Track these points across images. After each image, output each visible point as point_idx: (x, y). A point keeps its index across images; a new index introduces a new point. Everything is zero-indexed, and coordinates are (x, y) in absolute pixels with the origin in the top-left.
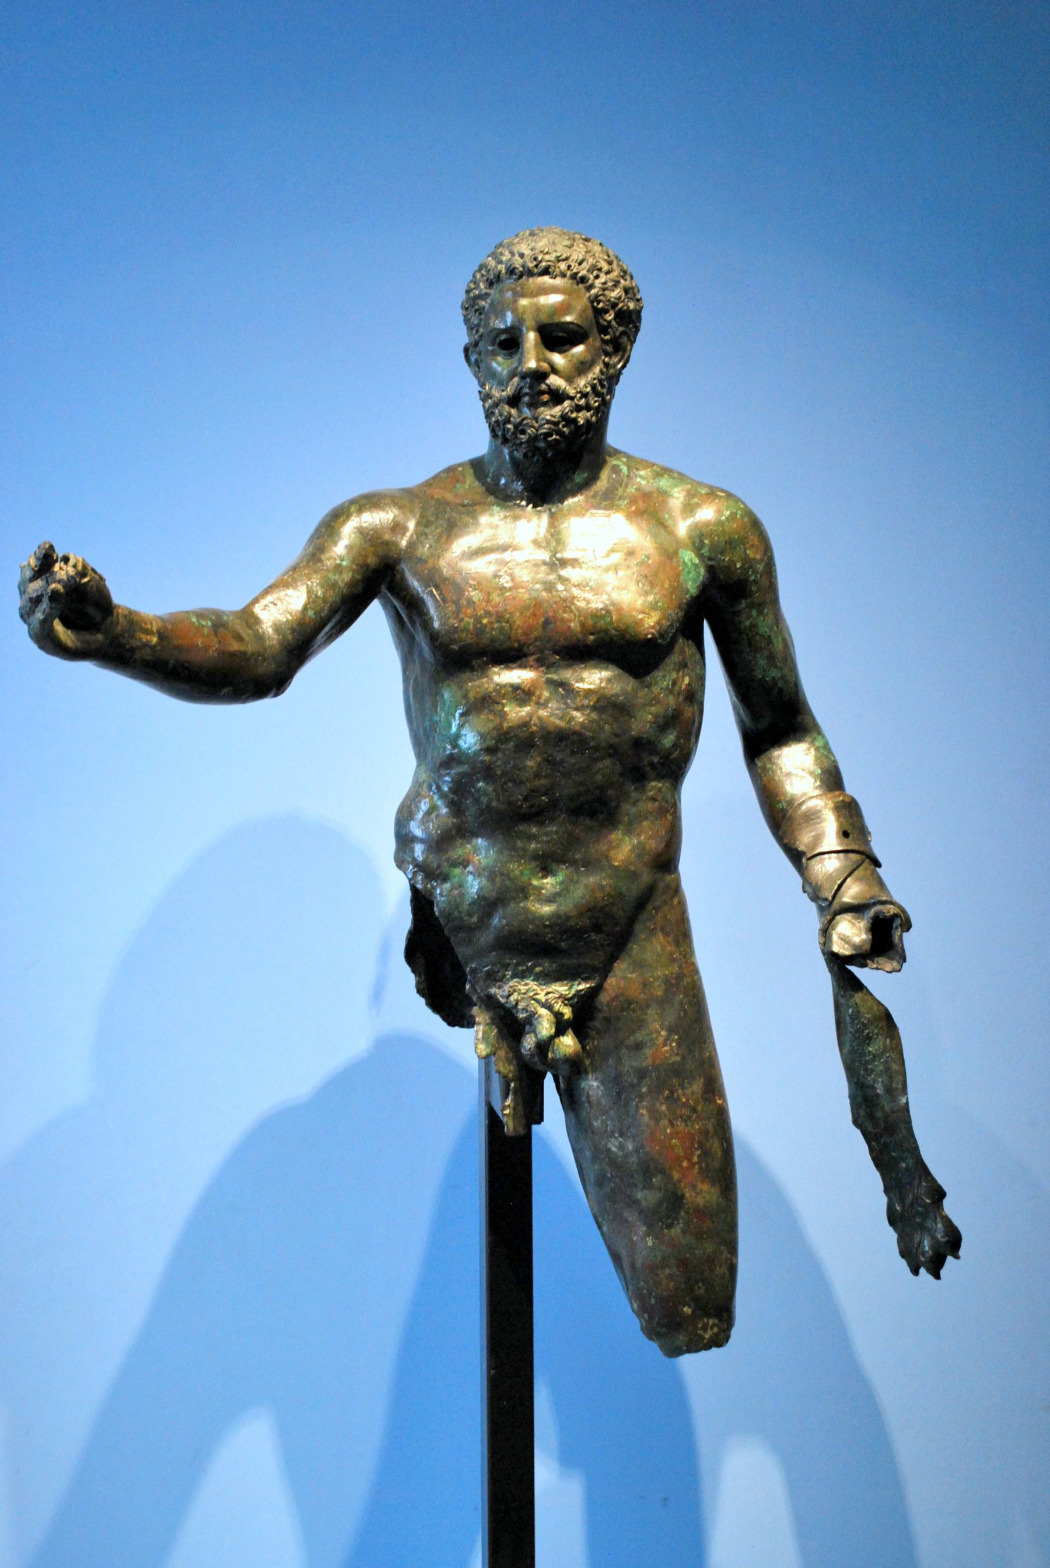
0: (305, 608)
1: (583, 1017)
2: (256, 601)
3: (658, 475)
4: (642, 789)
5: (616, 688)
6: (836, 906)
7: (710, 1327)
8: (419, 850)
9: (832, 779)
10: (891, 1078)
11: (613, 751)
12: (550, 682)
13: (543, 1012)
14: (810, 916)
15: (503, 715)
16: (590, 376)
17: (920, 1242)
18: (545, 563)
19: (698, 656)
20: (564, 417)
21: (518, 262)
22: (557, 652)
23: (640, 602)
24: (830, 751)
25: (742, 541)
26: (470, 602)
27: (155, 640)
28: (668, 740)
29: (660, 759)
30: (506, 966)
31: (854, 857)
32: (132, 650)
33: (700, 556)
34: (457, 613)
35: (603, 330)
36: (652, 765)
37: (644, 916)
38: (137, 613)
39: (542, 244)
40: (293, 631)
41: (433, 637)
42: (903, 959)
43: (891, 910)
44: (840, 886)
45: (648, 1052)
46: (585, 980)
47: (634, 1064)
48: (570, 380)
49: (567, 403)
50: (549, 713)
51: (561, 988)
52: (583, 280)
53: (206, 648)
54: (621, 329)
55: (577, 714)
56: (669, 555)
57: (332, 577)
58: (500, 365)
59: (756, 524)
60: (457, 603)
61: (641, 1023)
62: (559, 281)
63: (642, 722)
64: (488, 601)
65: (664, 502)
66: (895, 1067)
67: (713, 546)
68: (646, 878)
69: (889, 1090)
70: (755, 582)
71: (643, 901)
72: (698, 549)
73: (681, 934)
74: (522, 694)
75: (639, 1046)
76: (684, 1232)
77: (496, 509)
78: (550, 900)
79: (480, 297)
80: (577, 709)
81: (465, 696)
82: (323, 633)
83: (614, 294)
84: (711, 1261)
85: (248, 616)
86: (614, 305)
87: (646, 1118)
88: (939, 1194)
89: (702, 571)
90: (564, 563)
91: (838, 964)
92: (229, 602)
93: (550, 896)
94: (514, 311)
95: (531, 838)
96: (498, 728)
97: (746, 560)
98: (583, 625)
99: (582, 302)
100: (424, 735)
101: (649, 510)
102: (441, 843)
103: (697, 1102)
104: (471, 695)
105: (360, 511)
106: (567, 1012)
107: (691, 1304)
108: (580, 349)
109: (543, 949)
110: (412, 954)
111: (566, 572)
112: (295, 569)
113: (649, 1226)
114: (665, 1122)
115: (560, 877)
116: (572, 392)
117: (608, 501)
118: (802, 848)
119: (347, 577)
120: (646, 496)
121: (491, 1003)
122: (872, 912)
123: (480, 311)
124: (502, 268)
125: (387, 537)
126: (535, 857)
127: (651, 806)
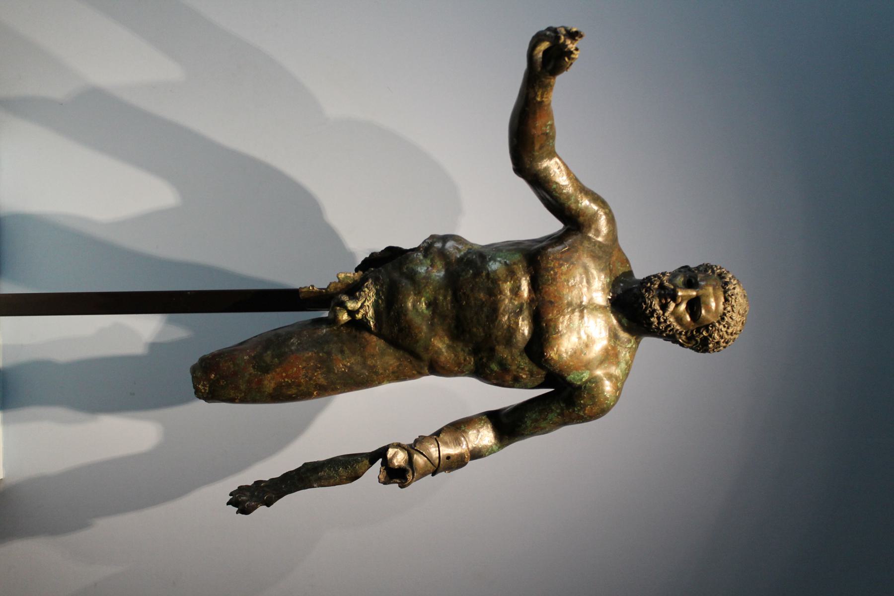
0: (557, 183)
1: (357, 324)
2: (560, 159)
3: (627, 363)
4: (469, 354)
5: (519, 338)
6: (412, 451)
7: (204, 388)
8: (438, 245)
9: (476, 454)
10: (326, 479)
11: (489, 336)
12: (521, 307)
13: (359, 304)
14: (408, 440)
15: (505, 282)
16: (675, 324)
17: (245, 495)
18: (581, 302)
19: (536, 384)
20: (654, 311)
21: (731, 287)
22: (537, 308)
23: (563, 349)
24: (490, 453)
25: (594, 404)
26: (562, 265)
27: (539, 99)
28: (494, 367)
29: (487, 368)
30: (382, 286)
31: (437, 461)
32: (533, 87)
33: (586, 382)
34: (555, 259)
35: (698, 330)
36: (481, 359)
37: (407, 356)
38: (552, 89)
39: (740, 299)
40: (546, 177)
41: (544, 248)
42: (385, 483)
43: (410, 477)
44: (422, 454)
45: (340, 356)
46: (375, 325)
47: (334, 350)
48: (673, 313)
49: (661, 312)
50: (507, 302)
51: (371, 313)
52: (723, 319)
53: (535, 128)
54: (699, 340)
55: (506, 317)
56: (588, 365)
57: (573, 198)
58: (680, 280)
59: (603, 411)
60: (561, 258)
61: (354, 353)
62: (721, 307)
63: (503, 352)
64: (562, 274)
65: (612, 363)
66: (332, 481)
67: (591, 389)
68: (426, 357)
69: (320, 479)
70: (574, 411)
71: (417, 357)
72: (589, 381)
73: (399, 376)
74: (516, 291)
75: (342, 352)
76: (250, 374)
77: (608, 280)
78: (414, 306)
79: (713, 272)
80: (509, 318)
81: (515, 264)
82: (545, 193)
83: (716, 335)
84: (237, 388)
85: (552, 154)
86: (710, 336)
87: (307, 355)
88: (269, 504)
89: (579, 383)
90: (582, 312)
91: (381, 453)
92: (559, 145)
93: (416, 306)
94: (707, 285)
95: (445, 297)
96: (499, 279)
97: (585, 406)
98: (551, 320)
99: (711, 318)
100: (497, 249)
101: (609, 356)
102: (443, 254)
103: (315, 381)
104: (515, 266)
105: (605, 214)
106: (359, 316)
107: (217, 379)
108: (688, 318)
109: (390, 305)
110: (390, 249)
111: (577, 314)
112: (576, 180)
113: (254, 358)
114: (304, 364)
115: (425, 312)
116: (667, 314)
117: (614, 336)
118: (441, 436)
119: (573, 206)
120: (617, 355)
121: (364, 280)
122: (408, 468)
123: (706, 271)
124: (728, 280)
125: (593, 226)
126: (436, 299)
127: (462, 358)
